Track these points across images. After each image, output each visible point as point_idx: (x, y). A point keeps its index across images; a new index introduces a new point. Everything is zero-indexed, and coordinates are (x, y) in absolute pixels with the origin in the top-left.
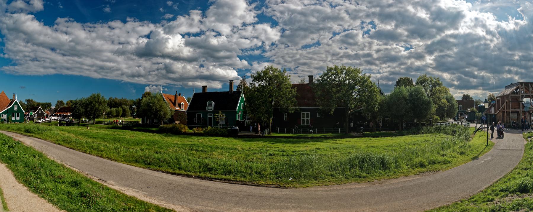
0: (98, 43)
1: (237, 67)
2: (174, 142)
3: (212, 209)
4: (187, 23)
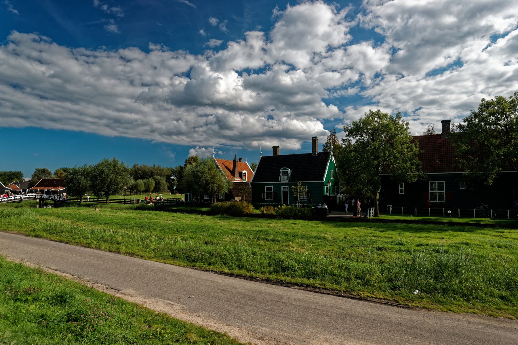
0: (105, 82)
1: (322, 117)
2: (233, 228)
3: (286, 334)
4: (244, 53)
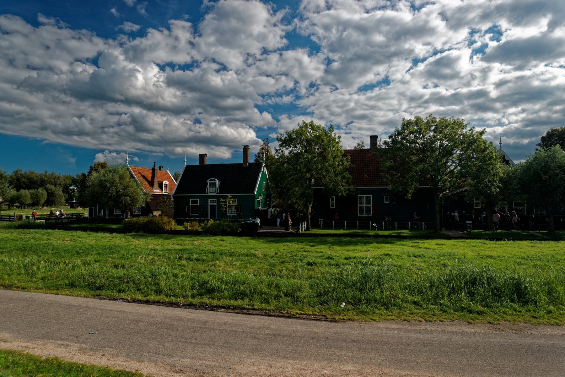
1: (255, 124)
2: (150, 247)
3: (209, 363)
4: (167, 44)
